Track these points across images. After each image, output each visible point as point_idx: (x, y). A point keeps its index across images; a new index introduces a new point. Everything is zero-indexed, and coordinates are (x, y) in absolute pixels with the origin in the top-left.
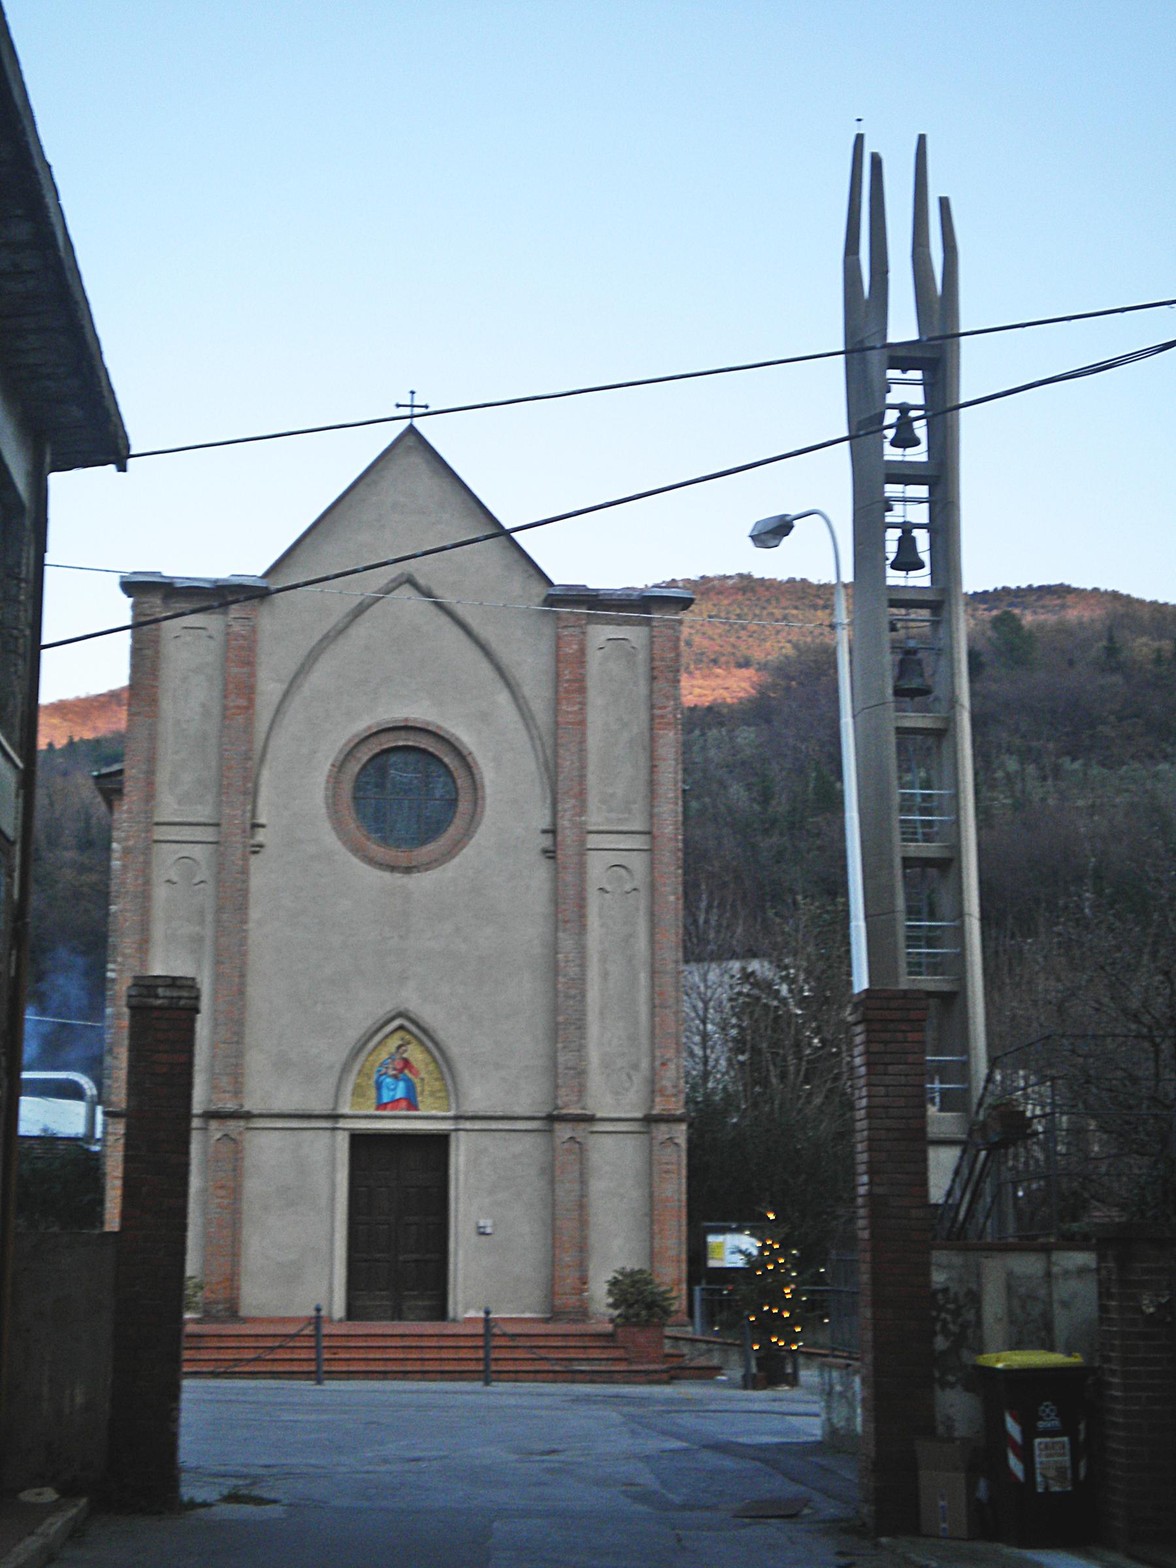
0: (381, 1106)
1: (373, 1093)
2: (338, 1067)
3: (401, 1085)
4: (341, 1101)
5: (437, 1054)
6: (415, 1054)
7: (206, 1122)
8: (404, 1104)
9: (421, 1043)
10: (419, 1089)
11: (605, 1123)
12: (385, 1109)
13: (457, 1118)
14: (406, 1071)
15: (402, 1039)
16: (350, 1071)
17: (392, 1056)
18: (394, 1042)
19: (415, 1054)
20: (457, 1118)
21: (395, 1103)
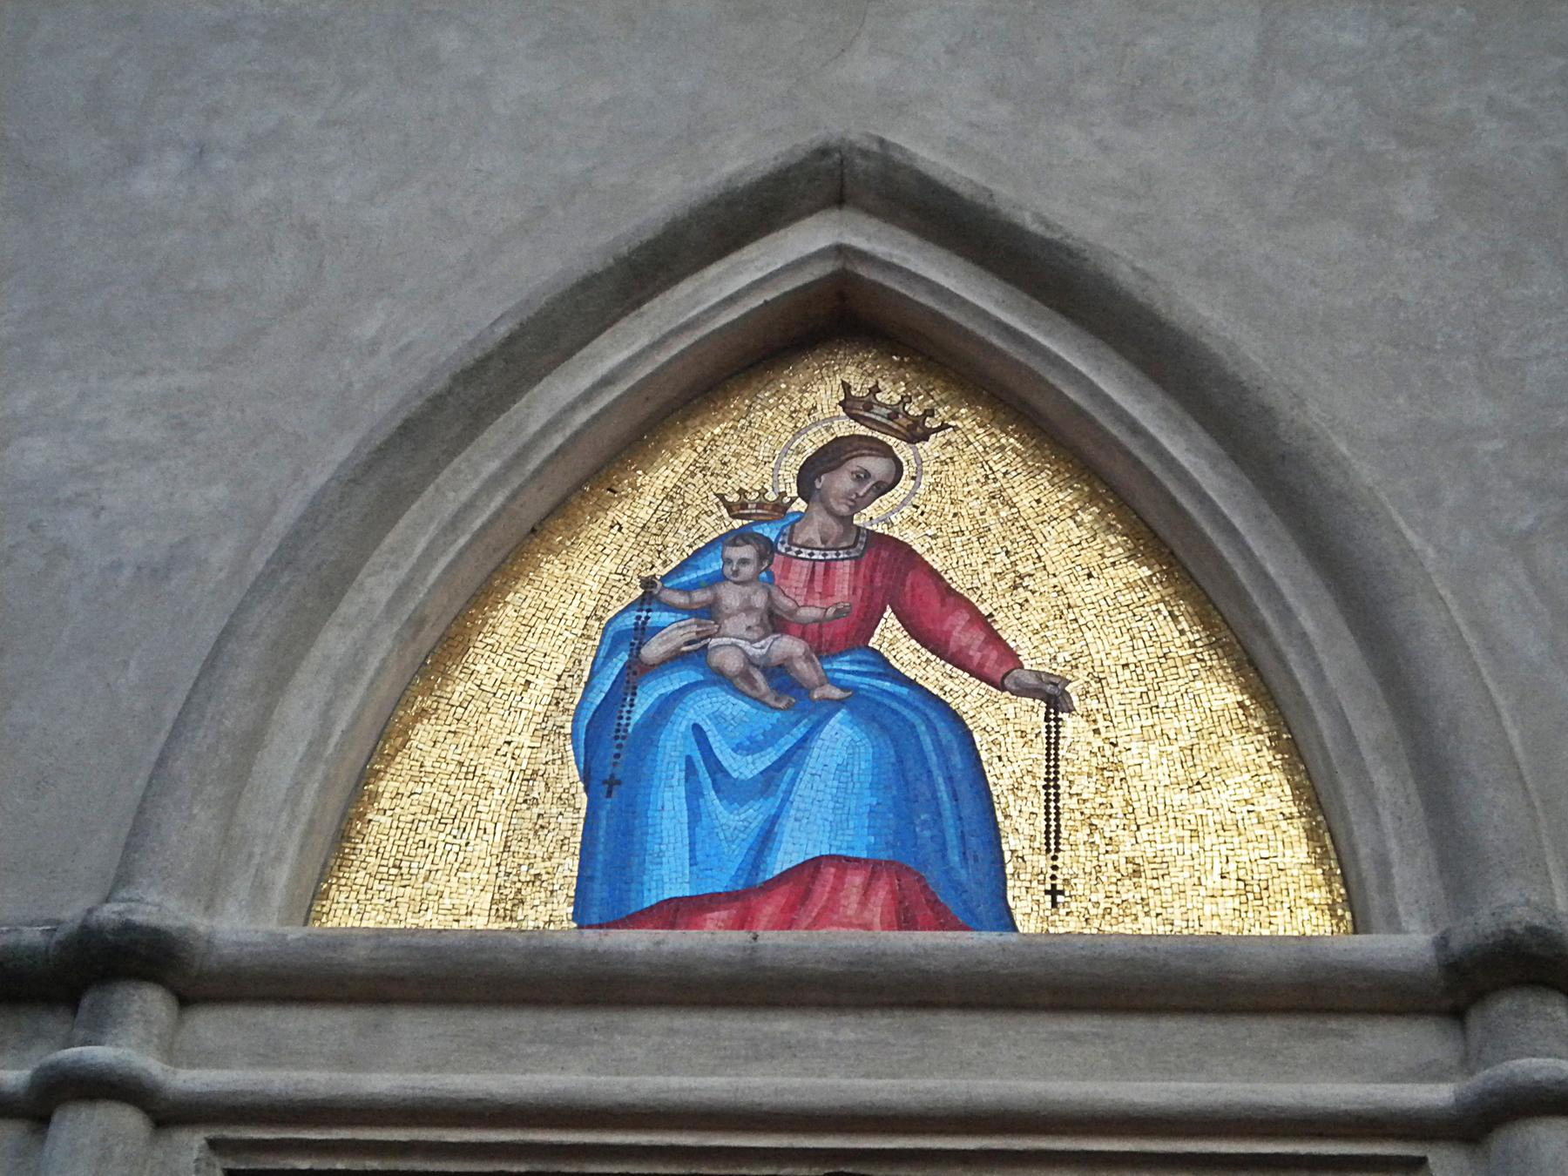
14: (890, 637)
15: (851, 406)
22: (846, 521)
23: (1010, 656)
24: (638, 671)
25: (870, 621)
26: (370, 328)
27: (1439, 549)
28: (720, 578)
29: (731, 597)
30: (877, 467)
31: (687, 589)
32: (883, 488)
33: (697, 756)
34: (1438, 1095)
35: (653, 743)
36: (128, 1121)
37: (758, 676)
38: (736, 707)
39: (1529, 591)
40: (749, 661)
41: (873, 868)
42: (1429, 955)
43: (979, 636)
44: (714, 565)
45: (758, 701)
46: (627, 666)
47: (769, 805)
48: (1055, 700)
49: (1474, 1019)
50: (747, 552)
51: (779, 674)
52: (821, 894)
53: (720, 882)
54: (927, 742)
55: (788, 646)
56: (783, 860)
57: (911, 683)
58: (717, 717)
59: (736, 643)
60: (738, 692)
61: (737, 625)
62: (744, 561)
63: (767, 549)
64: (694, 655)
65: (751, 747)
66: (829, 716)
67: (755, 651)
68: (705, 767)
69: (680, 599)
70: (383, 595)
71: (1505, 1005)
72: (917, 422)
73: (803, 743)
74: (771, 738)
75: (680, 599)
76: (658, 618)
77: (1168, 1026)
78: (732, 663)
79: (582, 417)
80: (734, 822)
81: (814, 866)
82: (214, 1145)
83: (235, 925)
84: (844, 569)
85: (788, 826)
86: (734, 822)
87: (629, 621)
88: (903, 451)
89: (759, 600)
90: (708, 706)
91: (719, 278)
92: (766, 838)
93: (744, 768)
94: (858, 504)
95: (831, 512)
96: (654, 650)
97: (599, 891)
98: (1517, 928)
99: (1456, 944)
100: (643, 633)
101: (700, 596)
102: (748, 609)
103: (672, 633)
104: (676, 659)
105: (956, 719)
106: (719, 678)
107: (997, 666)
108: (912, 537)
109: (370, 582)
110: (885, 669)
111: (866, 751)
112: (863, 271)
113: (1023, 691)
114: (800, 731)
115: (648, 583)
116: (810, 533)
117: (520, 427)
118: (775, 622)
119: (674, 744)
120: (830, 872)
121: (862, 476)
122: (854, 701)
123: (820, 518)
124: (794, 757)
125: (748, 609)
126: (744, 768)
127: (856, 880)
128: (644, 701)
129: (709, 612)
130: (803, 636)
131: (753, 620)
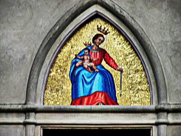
0: (76, 99)
1: (68, 87)
2: (30, 58)
3: (98, 77)
4: (32, 94)
5: (136, 43)
6: (115, 45)
7: (18, 105)
8: (101, 97)
9: (121, 33)
10: (117, 83)
11: (9, 115)
12: (81, 103)
13: (157, 111)
14: (104, 63)
15: (99, 29)
16: (54, 56)
17: (88, 48)
18: (88, 33)
19: (115, 45)
20: (157, 111)
21: (91, 97)
22: (98, 46)
23: (117, 66)
24: (76, 68)
25: (101, 61)
26: (40, 23)
27: (162, 59)
28: (84, 55)
29: (85, 57)
30: (102, 38)
31: (81, 56)
32: (102, 42)
33: (83, 80)
34: (153, 122)
35: (78, 76)
36: (34, 126)
37: (89, 68)
38: (87, 72)
39: (170, 64)
40: (88, 66)
41: (102, 92)
42: (154, 109)
43: (113, 63)
44: (83, 53)
45: (89, 72)
46: (74, 67)
47: (91, 85)
48: (121, 71)
49: (158, 114)
50: (87, 51)
51: (91, 68)
52: (97, 95)
53: (86, 94)
54: (107, 76)
55: (92, 64)
56: (93, 91)
57: (106, 70)
58: (85, 74)
59: (87, 64)
60: (87, 70)
61: (86, 61)
62: (87, 52)
63: (89, 51)
64: (82, 65)
65: (89, 78)
66: (96, 75)
67: (89, 65)
68: (84, 80)
69: (80, 58)
70: (48, 63)
71: (161, 113)
72: (106, 32)
73: (94, 77)
74: (92, 75)
75: (80, 58)
76: (77, 60)
77: (130, 114)
78: (86, 67)
79: (67, 36)
80: (88, 87)
81: (96, 93)
82: (41, 127)
83: (39, 105)
84: (98, 54)
85: (93, 87)
86: (88, 87)
87: (74, 61)
88: (104, 36)
89: (89, 58)
90: (84, 72)
91: (82, 16)
92: (91, 89)
93: (88, 80)
94: (100, 44)
95: (96, 45)
96: (77, 65)
97: (74, 96)
98: (162, 108)
99: (156, 108)
100: (76, 62)
101: (82, 57)
102: (87, 59)
103: (79, 63)
104: (80, 66)
105: (111, 74)
106: (84, 68)
107: (115, 66)
108: (107, 50)
109: (46, 61)
110: (103, 67)
111: (101, 78)
112: (99, 14)
113: (118, 70)
114: (94, 75)
115: (76, 55)
116: (94, 48)
117: (60, 40)
118: (91, 61)
119: (80, 77)
120: (98, 93)
121: (100, 40)
122: (100, 72)
123: (95, 46)
124: (94, 79)
125: (87, 59)
126: (88, 80)
127: (100, 94)
128: (77, 72)
129: (83, 60)
130: (94, 63)
131: (88, 61)
